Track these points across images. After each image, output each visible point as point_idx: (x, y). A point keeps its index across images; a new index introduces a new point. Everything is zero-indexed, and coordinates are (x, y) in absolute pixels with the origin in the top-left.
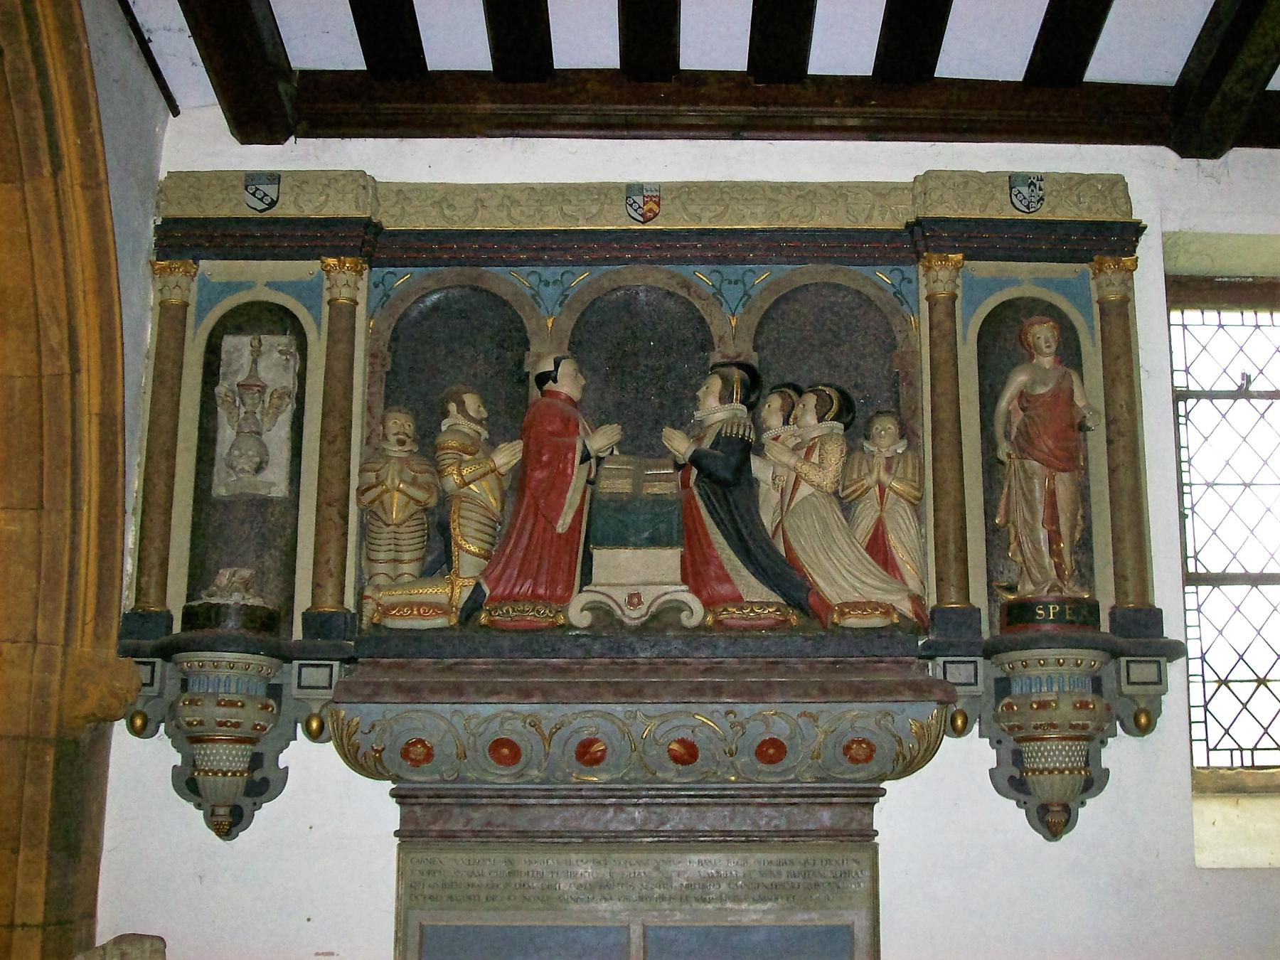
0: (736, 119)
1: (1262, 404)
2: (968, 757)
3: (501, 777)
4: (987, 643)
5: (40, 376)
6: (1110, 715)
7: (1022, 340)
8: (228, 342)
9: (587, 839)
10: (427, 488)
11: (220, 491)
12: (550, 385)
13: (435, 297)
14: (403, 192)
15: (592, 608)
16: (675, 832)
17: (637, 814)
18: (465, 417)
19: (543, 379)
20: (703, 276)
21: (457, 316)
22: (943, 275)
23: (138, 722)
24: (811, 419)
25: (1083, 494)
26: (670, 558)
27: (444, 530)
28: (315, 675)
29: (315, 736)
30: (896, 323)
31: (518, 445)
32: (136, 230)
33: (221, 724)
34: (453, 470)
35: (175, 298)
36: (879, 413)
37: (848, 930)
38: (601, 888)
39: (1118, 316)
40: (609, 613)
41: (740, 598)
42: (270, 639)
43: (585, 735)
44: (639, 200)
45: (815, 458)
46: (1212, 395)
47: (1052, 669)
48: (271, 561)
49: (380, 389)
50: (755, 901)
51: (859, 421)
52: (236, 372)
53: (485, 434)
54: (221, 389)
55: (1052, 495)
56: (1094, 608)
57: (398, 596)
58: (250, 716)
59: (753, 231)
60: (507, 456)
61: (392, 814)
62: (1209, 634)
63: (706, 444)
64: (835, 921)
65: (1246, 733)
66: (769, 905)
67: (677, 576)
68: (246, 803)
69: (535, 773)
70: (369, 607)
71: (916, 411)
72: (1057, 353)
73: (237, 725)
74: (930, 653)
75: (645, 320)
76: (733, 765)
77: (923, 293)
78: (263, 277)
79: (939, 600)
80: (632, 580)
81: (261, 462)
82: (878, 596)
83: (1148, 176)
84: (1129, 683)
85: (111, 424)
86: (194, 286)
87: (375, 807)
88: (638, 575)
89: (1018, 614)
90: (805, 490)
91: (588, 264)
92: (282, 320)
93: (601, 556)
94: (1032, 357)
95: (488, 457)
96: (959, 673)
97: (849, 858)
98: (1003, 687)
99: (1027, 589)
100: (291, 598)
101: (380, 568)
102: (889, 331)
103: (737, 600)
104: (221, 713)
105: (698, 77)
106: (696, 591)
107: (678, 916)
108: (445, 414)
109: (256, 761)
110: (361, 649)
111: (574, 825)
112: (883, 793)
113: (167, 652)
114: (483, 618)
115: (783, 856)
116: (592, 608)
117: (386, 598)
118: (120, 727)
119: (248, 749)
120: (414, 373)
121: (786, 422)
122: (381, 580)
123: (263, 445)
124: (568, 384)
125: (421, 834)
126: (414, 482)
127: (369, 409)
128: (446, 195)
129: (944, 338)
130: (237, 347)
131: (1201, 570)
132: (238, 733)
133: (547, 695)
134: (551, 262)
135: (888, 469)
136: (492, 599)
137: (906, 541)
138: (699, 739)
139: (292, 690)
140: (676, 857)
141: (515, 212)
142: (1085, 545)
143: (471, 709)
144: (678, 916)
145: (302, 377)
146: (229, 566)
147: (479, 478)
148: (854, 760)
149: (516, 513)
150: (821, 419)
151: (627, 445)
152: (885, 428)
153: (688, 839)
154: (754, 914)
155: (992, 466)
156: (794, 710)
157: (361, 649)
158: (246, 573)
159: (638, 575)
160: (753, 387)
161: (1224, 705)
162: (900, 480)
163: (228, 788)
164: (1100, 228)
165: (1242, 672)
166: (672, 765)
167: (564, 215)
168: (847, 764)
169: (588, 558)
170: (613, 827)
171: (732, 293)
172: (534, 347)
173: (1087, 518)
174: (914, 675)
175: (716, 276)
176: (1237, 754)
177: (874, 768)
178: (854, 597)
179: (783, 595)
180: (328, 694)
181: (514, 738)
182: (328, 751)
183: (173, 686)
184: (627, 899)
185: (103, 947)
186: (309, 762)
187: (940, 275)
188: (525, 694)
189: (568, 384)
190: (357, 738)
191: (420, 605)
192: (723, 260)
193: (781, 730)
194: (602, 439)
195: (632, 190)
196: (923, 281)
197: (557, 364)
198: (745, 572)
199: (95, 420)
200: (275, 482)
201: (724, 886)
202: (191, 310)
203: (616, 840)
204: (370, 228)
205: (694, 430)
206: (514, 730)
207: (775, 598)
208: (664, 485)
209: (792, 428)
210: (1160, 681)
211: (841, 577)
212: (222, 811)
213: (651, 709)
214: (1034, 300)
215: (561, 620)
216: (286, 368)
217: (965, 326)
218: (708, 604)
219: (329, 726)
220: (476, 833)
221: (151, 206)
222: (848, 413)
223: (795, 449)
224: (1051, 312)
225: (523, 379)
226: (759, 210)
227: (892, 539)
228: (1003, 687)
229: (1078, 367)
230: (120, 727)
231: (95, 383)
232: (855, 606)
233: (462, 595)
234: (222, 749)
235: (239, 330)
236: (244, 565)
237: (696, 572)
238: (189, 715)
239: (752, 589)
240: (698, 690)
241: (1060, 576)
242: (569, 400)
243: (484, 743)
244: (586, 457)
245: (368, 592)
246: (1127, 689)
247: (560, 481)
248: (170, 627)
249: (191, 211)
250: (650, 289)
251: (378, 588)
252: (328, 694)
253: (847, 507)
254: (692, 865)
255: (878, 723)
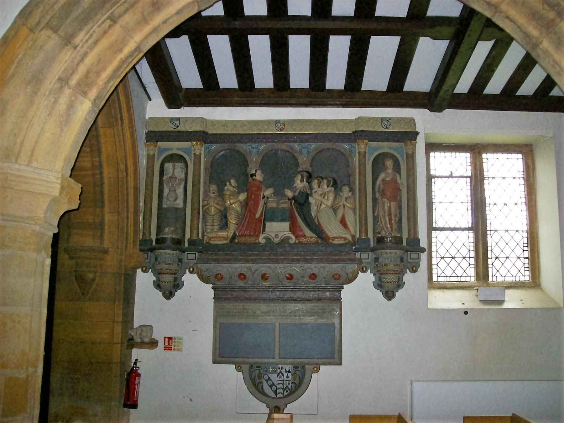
0: (307, 102)
1: (456, 179)
2: (366, 279)
3: (241, 283)
4: (373, 247)
5: (118, 178)
6: (406, 267)
7: (384, 164)
8: (166, 165)
9: (264, 300)
10: (221, 205)
11: (165, 206)
12: (254, 177)
13: (223, 152)
14: (214, 123)
15: (266, 238)
16: (287, 298)
17: (278, 293)
18: (231, 186)
19: (252, 175)
20: (296, 146)
21: (229, 156)
22: (362, 147)
23: (144, 269)
24: (325, 187)
25: (400, 207)
26: (286, 225)
27: (226, 217)
28: (191, 256)
29: (191, 272)
30: (350, 160)
31: (246, 194)
32: (141, 134)
33: (167, 269)
34: (228, 201)
35: (152, 153)
36: (344, 185)
37: (333, 324)
38: (268, 313)
39: (411, 158)
40: (270, 239)
41: (305, 235)
42: (179, 246)
43: (263, 272)
44: (279, 125)
45: (326, 197)
46: (442, 177)
47: (389, 255)
48: (179, 225)
49: (208, 178)
50: (309, 316)
51: (339, 187)
52: (168, 174)
53: (237, 190)
54: (165, 178)
55: (390, 208)
56: (401, 239)
57: (213, 235)
58: (174, 267)
59: (310, 134)
60: (242, 197)
61: (212, 293)
62: (439, 244)
63: (296, 194)
64: (330, 322)
65: (448, 272)
66: (313, 318)
67: (288, 230)
68: (173, 290)
69: (250, 282)
70: (206, 238)
71: (354, 183)
72: (393, 169)
73: (171, 270)
74: (357, 250)
75: (280, 156)
76: (303, 280)
77: (357, 151)
78: (175, 147)
79: (360, 235)
80: (277, 230)
81: (176, 198)
82: (343, 236)
83: (420, 117)
84: (410, 259)
85: (136, 190)
86: (156, 149)
87: (208, 291)
88: (278, 229)
89: (380, 240)
90: (323, 206)
91: (266, 143)
92: (181, 158)
93: (268, 224)
94: (386, 169)
95: (237, 197)
96: (364, 256)
97: (335, 306)
98: (376, 259)
99: (383, 233)
100: (184, 235)
101: (208, 227)
102: (348, 162)
103: (304, 236)
104: (167, 266)
105: (295, 90)
106: (293, 233)
107: (288, 320)
108: (226, 185)
109: (176, 279)
110: (204, 250)
111: (261, 296)
112: (343, 288)
113: (152, 250)
114: (236, 241)
115: (316, 304)
116: (266, 238)
117: (210, 235)
118: (139, 270)
119: (174, 276)
120: (218, 173)
121: (319, 187)
122: (209, 231)
123: (176, 194)
124: (259, 177)
125: (220, 299)
126: (217, 204)
127: (205, 183)
128: (225, 123)
129: (362, 164)
130: (169, 166)
131: (437, 227)
132: (171, 272)
133: (253, 261)
134: (255, 142)
135: (346, 201)
136: (239, 236)
137: (350, 219)
138: (293, 273)
139: (185, 260)
140: (288, 304)
141: (245, 128)
142: (400, 221)
143: (233, 265)
144: (288, 320)
145: (186, 174)
146: (168, 227)
147: (235, 203)
148: (335, 279)
149: (245, 212)
150: (328, 187)
151: (276, 194)
152: (346, 189)
153: (291, 300)
154: (309, 320)
155: (375, 200)
156: (319, 266)
157: (204, 250)
158: (172, 229)
159: (278, 229)
160: (310, 177)
161: (442, 264)
162: (350, 204)
163: (169, 286)
164: (406, 133)
165: (448, 255)
166: (287, 281)
167: (258, 129)
168: (333, 281)
169: (264, 225)
170: (271, 297)
171: (305, 151)
172: (250, 166)
173: (400, 213)
174: (352, 256)
175: (300, 146)
176: (445, 278)
177: (341, 281)
178: (336, 235)
179: (317, 234)
180: (195, 261)
181: (244, 273)
182: (195, 276)
183: (153, 259)
184: (275, 316)
185: (136, 328)
186: (190, 280)
187: (362, 146)
188: (247, 261)
189: (259, 177)
190: (203, 273)
191: (219, 237)
192: (302, 142)
193: (316, 271)
194: (268, 192)
195: (277, 122)
196: (357, 148)
197: (256, 172)
198: (306, 228)
199: (132, 188)
200: (180, 203)
201: (300, 312)
202: (156, 156)
203: (271, 300)
204: (205, 133)
205: (293, 189)
206: (244, 271)
207: (315, 235)
208: (285, 205)
209: (320, 189)
210: (419, 258)
211: (333, 230)
212: (167, 292)
213: (280, 265)
214: (387, 153)
215: (257, 241)
216: (182, 172)
217: (369, 160)
218: (297, 237)
219: (195, 270)
220: (234, 298)
221: (144, 127)
222: (335, 184)
223: (321, 194)
224: (393, 157)
225: (247, 175)
226: (312, 127)
227: (347, 220)
228: (376, 259)
229: (399, 173)
230: (139, 270)
231: (132, 179)
232: (336, 238)
233: (231, 235)
234: (167, 276)
235: (168, 162)
236: (171, 226)
237: (293, 228)
238: (158, 267)
239: (308, 233)
240: (293, 260)
241: (392, 230)
242: (260, 182)
243: (237, 274)
244: (264, 197)
245: (205, 234)
246: (410, 260)
247: (257, 203)
248: (152, 244)
249: (156, 129)
250: (282, 150)
251: (208, 233)
252: (195, 261)
253: (335, 209)
254: (292, 307)
255: (341, 269)
